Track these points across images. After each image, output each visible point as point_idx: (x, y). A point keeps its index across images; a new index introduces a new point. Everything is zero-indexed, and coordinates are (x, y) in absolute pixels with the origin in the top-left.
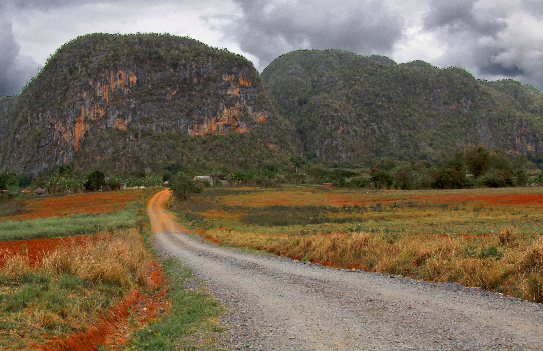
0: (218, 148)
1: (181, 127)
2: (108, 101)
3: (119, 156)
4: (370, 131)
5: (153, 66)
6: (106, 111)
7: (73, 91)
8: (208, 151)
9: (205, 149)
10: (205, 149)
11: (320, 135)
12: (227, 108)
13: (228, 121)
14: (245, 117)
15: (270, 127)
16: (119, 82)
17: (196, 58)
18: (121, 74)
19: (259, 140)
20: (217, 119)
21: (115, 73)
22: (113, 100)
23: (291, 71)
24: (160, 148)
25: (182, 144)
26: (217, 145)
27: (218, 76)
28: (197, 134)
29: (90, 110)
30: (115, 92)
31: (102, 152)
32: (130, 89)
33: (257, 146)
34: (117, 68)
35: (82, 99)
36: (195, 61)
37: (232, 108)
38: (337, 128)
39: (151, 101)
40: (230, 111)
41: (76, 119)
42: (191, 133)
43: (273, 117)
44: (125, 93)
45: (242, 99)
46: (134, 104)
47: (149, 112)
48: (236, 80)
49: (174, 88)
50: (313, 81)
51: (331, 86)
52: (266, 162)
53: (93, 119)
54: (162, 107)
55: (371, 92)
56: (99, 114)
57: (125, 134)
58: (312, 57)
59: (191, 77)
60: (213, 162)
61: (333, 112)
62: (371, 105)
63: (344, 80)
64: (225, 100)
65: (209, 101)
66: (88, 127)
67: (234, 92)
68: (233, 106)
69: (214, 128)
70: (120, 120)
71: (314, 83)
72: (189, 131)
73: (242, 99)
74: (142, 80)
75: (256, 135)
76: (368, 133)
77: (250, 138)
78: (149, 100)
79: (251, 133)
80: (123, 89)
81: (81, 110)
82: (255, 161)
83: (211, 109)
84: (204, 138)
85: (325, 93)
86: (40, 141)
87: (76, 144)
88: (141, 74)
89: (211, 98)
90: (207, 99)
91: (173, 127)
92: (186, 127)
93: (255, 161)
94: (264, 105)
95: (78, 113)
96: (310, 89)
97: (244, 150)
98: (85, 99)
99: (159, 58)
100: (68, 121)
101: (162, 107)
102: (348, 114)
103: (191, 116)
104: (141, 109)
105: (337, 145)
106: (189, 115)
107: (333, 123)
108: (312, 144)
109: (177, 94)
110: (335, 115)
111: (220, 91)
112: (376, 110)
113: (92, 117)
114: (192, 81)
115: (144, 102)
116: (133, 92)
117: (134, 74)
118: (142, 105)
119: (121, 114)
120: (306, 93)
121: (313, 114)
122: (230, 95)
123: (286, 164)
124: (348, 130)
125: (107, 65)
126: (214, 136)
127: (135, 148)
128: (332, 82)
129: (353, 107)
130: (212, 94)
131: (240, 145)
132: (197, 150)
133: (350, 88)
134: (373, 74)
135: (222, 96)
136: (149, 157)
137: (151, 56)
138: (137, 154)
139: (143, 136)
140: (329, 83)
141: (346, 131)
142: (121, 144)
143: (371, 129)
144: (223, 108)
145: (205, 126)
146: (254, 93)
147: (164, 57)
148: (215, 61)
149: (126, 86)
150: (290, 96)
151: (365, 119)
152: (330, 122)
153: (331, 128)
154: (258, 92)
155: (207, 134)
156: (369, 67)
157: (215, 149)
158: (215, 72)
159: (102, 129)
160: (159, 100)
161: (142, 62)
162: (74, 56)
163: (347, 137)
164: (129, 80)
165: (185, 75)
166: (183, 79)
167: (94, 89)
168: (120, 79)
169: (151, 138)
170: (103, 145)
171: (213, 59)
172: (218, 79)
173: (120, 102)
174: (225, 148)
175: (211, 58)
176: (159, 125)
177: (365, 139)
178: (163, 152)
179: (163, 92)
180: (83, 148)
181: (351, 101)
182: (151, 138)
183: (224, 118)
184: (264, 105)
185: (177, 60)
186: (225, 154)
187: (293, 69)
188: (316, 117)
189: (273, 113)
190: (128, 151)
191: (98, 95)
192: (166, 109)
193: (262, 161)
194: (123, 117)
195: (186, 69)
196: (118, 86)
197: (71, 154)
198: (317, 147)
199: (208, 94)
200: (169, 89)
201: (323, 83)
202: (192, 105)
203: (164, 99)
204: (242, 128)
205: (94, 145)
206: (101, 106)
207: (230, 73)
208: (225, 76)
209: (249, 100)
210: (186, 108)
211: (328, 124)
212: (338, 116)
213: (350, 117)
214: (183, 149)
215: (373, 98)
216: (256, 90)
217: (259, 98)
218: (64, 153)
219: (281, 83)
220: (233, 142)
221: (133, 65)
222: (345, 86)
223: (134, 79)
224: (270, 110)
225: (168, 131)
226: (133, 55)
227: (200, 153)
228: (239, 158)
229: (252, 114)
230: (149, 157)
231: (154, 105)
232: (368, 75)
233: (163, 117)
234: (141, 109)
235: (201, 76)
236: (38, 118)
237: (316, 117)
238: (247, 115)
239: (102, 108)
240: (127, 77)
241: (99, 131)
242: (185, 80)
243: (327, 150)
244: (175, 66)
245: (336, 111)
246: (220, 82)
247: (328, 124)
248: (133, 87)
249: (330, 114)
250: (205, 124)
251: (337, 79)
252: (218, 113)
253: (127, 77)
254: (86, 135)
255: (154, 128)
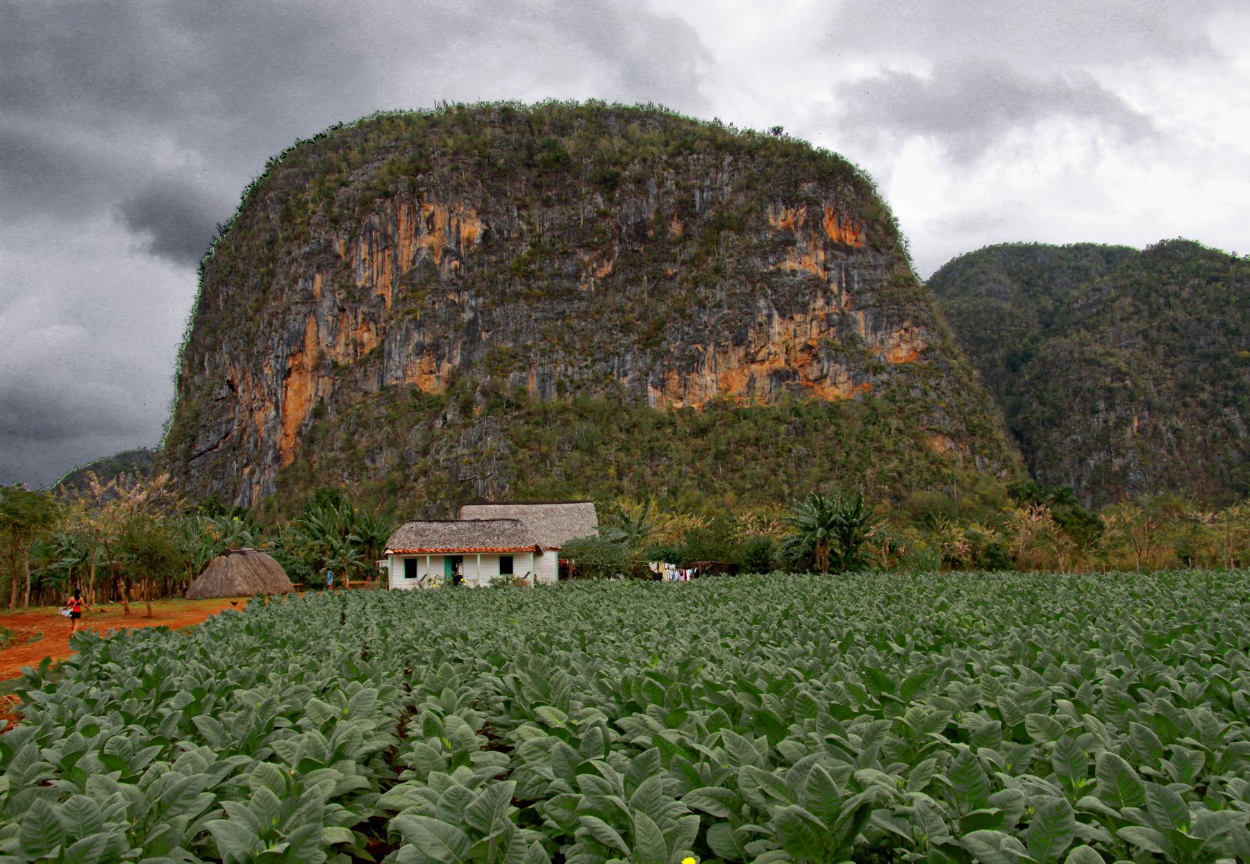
0: (750, 450)
1: (625, 381)
2: (389, 302)
3: (406, 477)
4: (1220, 432)
5: (538, 187)
6: (384, 333)
7: (287, 275)
8: (710, 460)
9: (700, 454)
10: (700, 454)
11: (1074, 441)
12: (782, 316)
13: (787, 361)
14: (846, 349)
15: (932, 382)
16: (426, 240)
17: (679, 159)
18: (433, 214)
19: (894, 423)
20: (747, 354)
21: (413, 212)
22: (405, 299)
23: (982, 289)
24: (544, 448)
25: (623, 436)
26: (743, 442)
27: (750, 211)
28: (680, 405)
29: (334, 332)
30: (411, 272)
31: (357, 467)
32: (462, 263)
33: (888, 443)
34: (420, 197)
35: (309, 298)
36: (677, 168)
37: (798, 318)
38: (1123, 422)
39: (527, 297)
40: (792, 326)
41: (290, 363)
42: (659, 401)
43: (943, 350)
44: (445, 275)
45: (834, 287)
46: (472, 308)
47: (518, 333)
48: (813, 225)
49: (603, 255)
50: (1042, 311)
51: (1098, 314)
52: (919, 496)
53: (342, 361)
54: (562, 315)
55: (1214, 325)
56: (362, 345)
57: (434, 406)
58: (1035, 259)
59: (662, 221)
60: (730, 496)
61: (1108, 380)
62: (1217, 357)
63: (1134, 297)
64: (775, 291)
65: (721, 295)
66: (325, 385)
67: (805, 262)
68: (804, 308)
69: (739, 386)
70: (425, 362)
71: (1045, 317)
72: (653, 394)
73: (834, 287)
74: (500, 232)
75: (884, 406)
76: (1214, 436)
77: (863, 418)
78: (518, 295)
79: (867, 401)
80: (437, 261)
81: (305, 333)
82: (881, 494)
83: (725, 321)
84: (704, 419)
85: (1083, 332)
86: (194, 439)
87: (287, 444)
88: (496, 213)
89: (727, 285)
90: (714, 287)
91: (597, 380)
92: (641, 380)
93: (881, 494)
94: (909, 308)
95: (297, 342)
96: (1036, 330)
97: (840, 457)
98: (318, 298)
99: (557, 160)
100: (266, 371)
101: (562, 315)
102: (1151, 382)
103: (658, 344)
104: (491, 325)
105: (1125, 469)
106: (650, 341)
107: (1111, 407)
108: (1051, 467)
109: (612, 275)
110: (1117, 385)
111: (757, 261)
112: (1234, 372)
113: (340, 353)
114: (664, 231)
115: (503, 299)
116: (470, 269)
117: (473, 213)
118: (497, 313)
119: (428, 341)
120: (1026, 340)
121: (1050, 386)
122: (794, 272)
123: (993, 504)
124: (1155, 428)
125: (391, 188)
126: (736, 413)
127: (460, 451)
128: (1099, 301)
129: (1166, 365)
130: (729, 270)
131: (827, 438)
132: (674, 455)
133: (1152, 316)
134: (1217, 280)
135: (765, 277)
136: (503, 481)
137: (531, 156)
138: (465, 471)
139: (491, 408)
140: (1092, 306)
141: (1150, 431)
142: (416, 437)
143: (1223, 425)
144: (770, 316)
145: (708, 378)
146: (875, 268)
147: (575, 160)
148: (740, 164)
149: (447, 252)
150: (983, 348)
151: (1204, 396)
152: (1102, 405)
153: (1105, 422)
154: (890, 266)
155: (714, 406)
156: (1202, 261)
157: (739, 453)
158: (741, 199)
159: (366, 393)
160: (552, 294)
161: (504, 174)
162: (305, 175)
163: (1150, 446)
164: (458, 232)
165: (639, 211)
166: (636, 225)
167: (348, 266)
168: (431, 232)
169: (519, 417)
170: (363, 443)
171: (736, 160)
172: (751, 223)
173: (428, 300)
174: (771, 449)
175: (729, 159)
176: (551, 376)
177: (1205, 451)
178: (552, 465)
179: (569, 267)
180: (308, 454)
181: (1160, 349)
182: (519, 417)
183: (773, 349)
184: (909, 308)
185: (615, 164)
186: (774, 471)
187: (990, 284)
188: (1061, 392)
189: (943, 336)
190: (437, 462)
191: (359, 284)
192: (574, 323)
193: (904, 493)
194: (435, 351)
195: (646, 194)
196: (424, 253)
197: (271, 475)
198: (1067, 475)
199: (717, 271)
200: (586, 258)
201: (1076, 306)
202: (662, 308)
203: (570, 291)
204: (834, 384)
205: (338, 445)
206: (370, 318)
207: (790, 203)
208: (776, 213)
209: (859, 293)
210: (643, 317)
211: (1095, 411)
212: (1125, 388)
213: (1159, 392)
214: (622, 455)
215: (1222, 339)
216: (882, 260)
217: (893, 284)
218: (252, 473)
219: (959, 315)
220: (800, 431)
221: (472, 185)
222: (1138, 311)
223: (473, 229)
224: (930, 325)
225: (579, 394)
226: (472, 156)
227: (684, 468)
228: (822, 485)
229: (870, 339)
230: (503, 481)
231: (535, 309)
232: (1203, 282)
233: (565, 347)
234: (491, 325)
235: (694, 216)
236: (202, 369)
237: (1061, 392)
238: (853, 340)
239: (372, 326)
240: (454, 223)
241: (359, 397)
242: (640, 231)
243: (1094, 483)
244: (609, 184)
245: (1118, 375)
246: (758, 231)
247: (1095, 411)
248: (471, 256)
249: (1100, 383)
250: (706, 371)
251: (1113, 293)
252: (751, 334)
253: (454, 223)
254: (318, 414)
255: (533, 385)
